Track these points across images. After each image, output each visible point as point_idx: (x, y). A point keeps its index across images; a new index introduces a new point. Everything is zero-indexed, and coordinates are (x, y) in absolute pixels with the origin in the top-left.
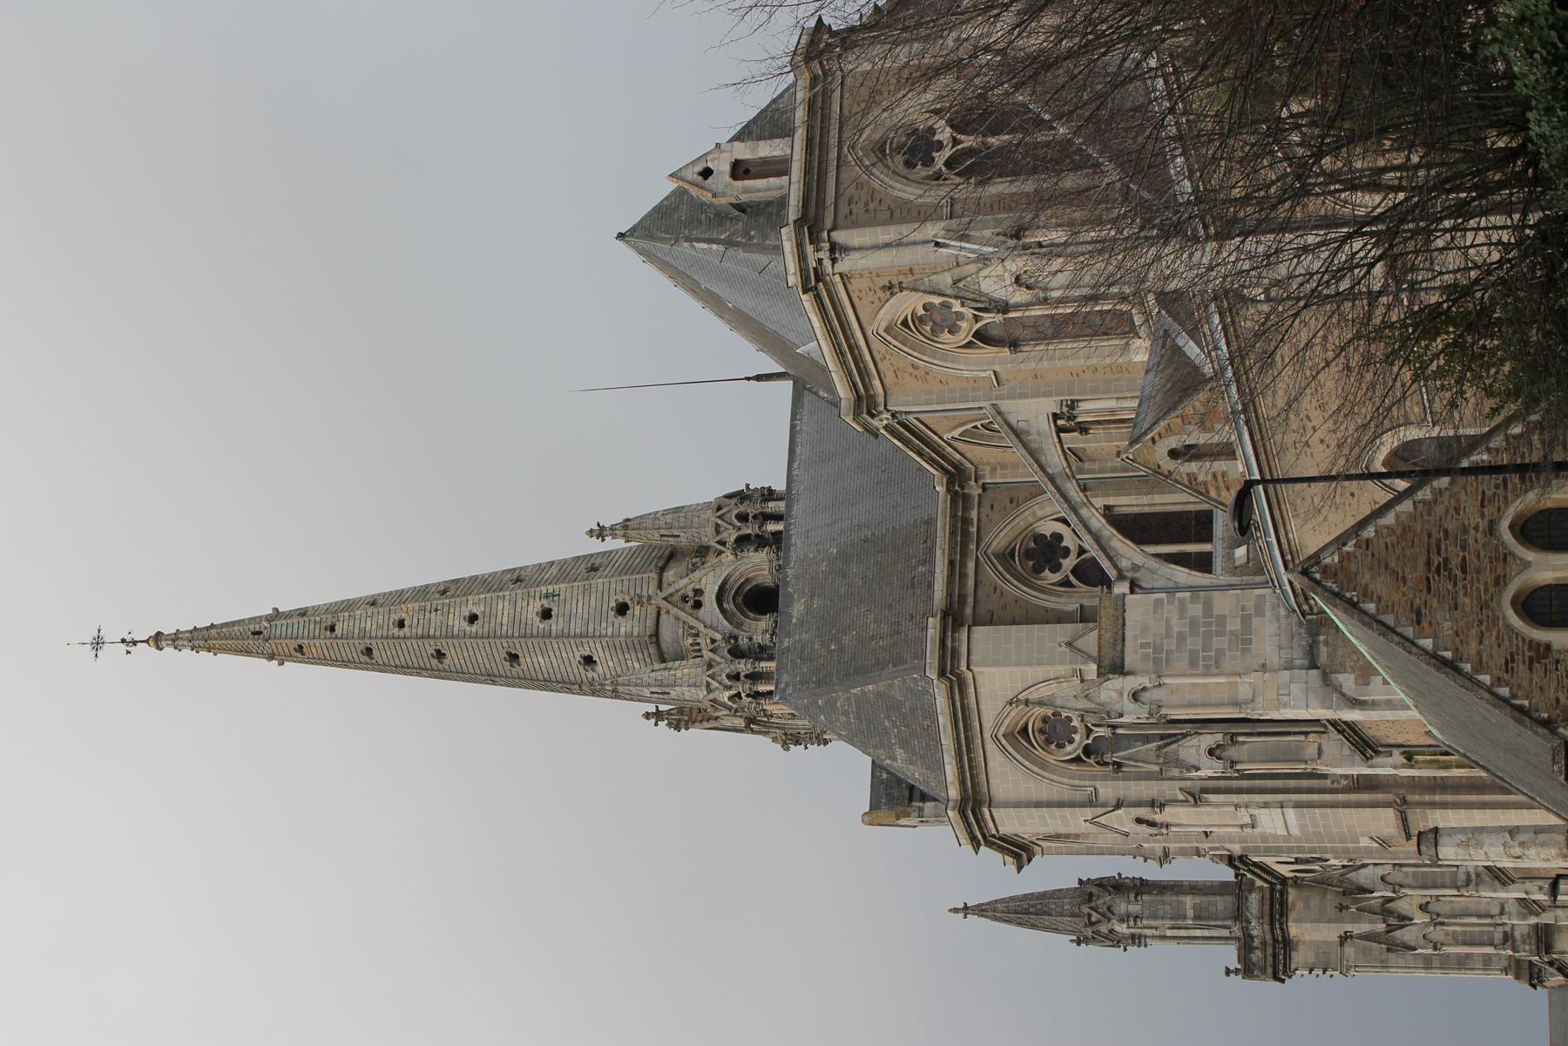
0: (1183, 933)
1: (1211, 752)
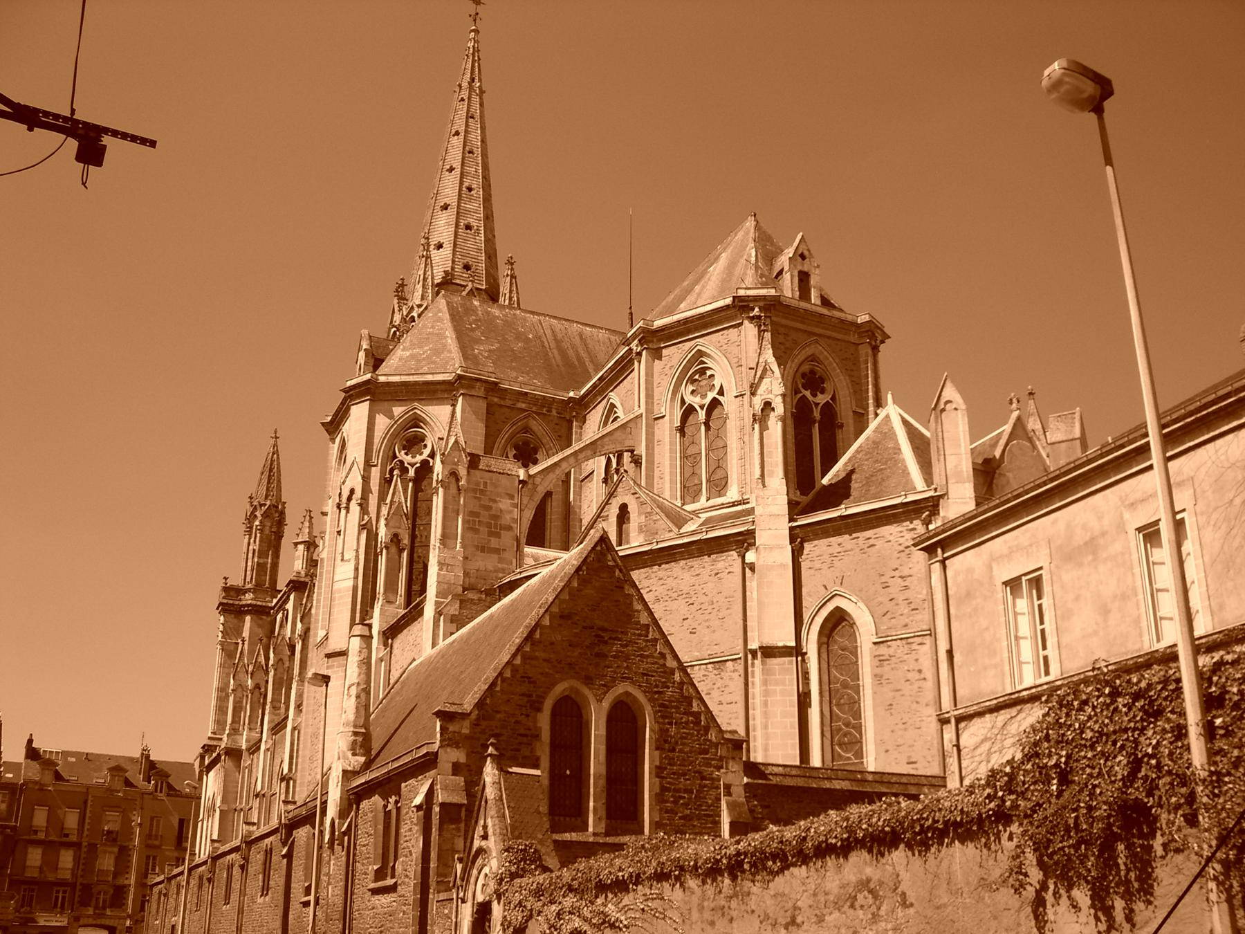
0: (250, 555)
1: (396, 535)
